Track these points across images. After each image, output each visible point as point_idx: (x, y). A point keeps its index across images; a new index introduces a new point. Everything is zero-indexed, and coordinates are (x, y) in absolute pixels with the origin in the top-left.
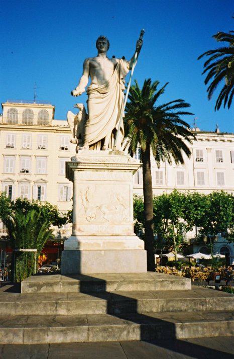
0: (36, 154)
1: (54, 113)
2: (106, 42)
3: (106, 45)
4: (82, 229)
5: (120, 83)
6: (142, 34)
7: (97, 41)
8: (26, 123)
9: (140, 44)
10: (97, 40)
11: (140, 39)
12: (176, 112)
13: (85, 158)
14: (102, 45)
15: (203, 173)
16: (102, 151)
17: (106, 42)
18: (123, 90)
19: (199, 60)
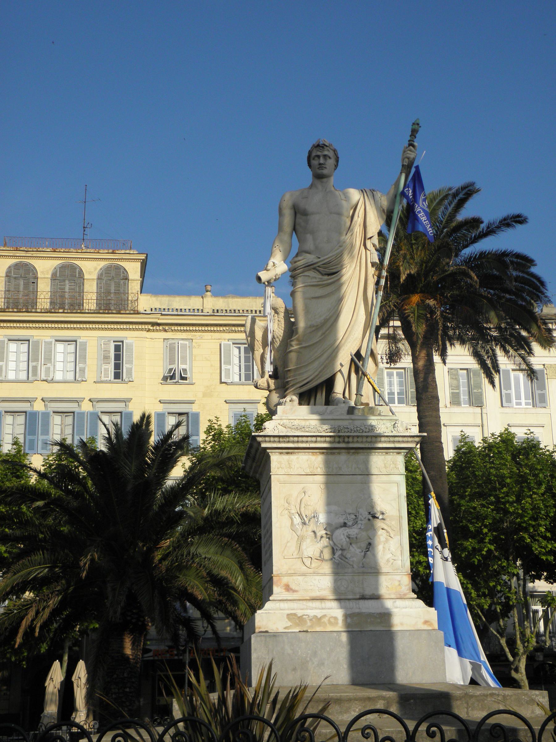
0: (45, 396)
1: (143, 275)
2: (331, 154)
3: (331, 162)
4: (293, 586)
5: (366, 248)
6: (414, 133)
7: (310, 153)
8: (62, 306)
9: (412, 155)
10: (309, 148)
11: (411, 145)
13: (296, 423)
14: (322, 161)
15: (115, 378)
16: (330, 408)
17: (331, 154)
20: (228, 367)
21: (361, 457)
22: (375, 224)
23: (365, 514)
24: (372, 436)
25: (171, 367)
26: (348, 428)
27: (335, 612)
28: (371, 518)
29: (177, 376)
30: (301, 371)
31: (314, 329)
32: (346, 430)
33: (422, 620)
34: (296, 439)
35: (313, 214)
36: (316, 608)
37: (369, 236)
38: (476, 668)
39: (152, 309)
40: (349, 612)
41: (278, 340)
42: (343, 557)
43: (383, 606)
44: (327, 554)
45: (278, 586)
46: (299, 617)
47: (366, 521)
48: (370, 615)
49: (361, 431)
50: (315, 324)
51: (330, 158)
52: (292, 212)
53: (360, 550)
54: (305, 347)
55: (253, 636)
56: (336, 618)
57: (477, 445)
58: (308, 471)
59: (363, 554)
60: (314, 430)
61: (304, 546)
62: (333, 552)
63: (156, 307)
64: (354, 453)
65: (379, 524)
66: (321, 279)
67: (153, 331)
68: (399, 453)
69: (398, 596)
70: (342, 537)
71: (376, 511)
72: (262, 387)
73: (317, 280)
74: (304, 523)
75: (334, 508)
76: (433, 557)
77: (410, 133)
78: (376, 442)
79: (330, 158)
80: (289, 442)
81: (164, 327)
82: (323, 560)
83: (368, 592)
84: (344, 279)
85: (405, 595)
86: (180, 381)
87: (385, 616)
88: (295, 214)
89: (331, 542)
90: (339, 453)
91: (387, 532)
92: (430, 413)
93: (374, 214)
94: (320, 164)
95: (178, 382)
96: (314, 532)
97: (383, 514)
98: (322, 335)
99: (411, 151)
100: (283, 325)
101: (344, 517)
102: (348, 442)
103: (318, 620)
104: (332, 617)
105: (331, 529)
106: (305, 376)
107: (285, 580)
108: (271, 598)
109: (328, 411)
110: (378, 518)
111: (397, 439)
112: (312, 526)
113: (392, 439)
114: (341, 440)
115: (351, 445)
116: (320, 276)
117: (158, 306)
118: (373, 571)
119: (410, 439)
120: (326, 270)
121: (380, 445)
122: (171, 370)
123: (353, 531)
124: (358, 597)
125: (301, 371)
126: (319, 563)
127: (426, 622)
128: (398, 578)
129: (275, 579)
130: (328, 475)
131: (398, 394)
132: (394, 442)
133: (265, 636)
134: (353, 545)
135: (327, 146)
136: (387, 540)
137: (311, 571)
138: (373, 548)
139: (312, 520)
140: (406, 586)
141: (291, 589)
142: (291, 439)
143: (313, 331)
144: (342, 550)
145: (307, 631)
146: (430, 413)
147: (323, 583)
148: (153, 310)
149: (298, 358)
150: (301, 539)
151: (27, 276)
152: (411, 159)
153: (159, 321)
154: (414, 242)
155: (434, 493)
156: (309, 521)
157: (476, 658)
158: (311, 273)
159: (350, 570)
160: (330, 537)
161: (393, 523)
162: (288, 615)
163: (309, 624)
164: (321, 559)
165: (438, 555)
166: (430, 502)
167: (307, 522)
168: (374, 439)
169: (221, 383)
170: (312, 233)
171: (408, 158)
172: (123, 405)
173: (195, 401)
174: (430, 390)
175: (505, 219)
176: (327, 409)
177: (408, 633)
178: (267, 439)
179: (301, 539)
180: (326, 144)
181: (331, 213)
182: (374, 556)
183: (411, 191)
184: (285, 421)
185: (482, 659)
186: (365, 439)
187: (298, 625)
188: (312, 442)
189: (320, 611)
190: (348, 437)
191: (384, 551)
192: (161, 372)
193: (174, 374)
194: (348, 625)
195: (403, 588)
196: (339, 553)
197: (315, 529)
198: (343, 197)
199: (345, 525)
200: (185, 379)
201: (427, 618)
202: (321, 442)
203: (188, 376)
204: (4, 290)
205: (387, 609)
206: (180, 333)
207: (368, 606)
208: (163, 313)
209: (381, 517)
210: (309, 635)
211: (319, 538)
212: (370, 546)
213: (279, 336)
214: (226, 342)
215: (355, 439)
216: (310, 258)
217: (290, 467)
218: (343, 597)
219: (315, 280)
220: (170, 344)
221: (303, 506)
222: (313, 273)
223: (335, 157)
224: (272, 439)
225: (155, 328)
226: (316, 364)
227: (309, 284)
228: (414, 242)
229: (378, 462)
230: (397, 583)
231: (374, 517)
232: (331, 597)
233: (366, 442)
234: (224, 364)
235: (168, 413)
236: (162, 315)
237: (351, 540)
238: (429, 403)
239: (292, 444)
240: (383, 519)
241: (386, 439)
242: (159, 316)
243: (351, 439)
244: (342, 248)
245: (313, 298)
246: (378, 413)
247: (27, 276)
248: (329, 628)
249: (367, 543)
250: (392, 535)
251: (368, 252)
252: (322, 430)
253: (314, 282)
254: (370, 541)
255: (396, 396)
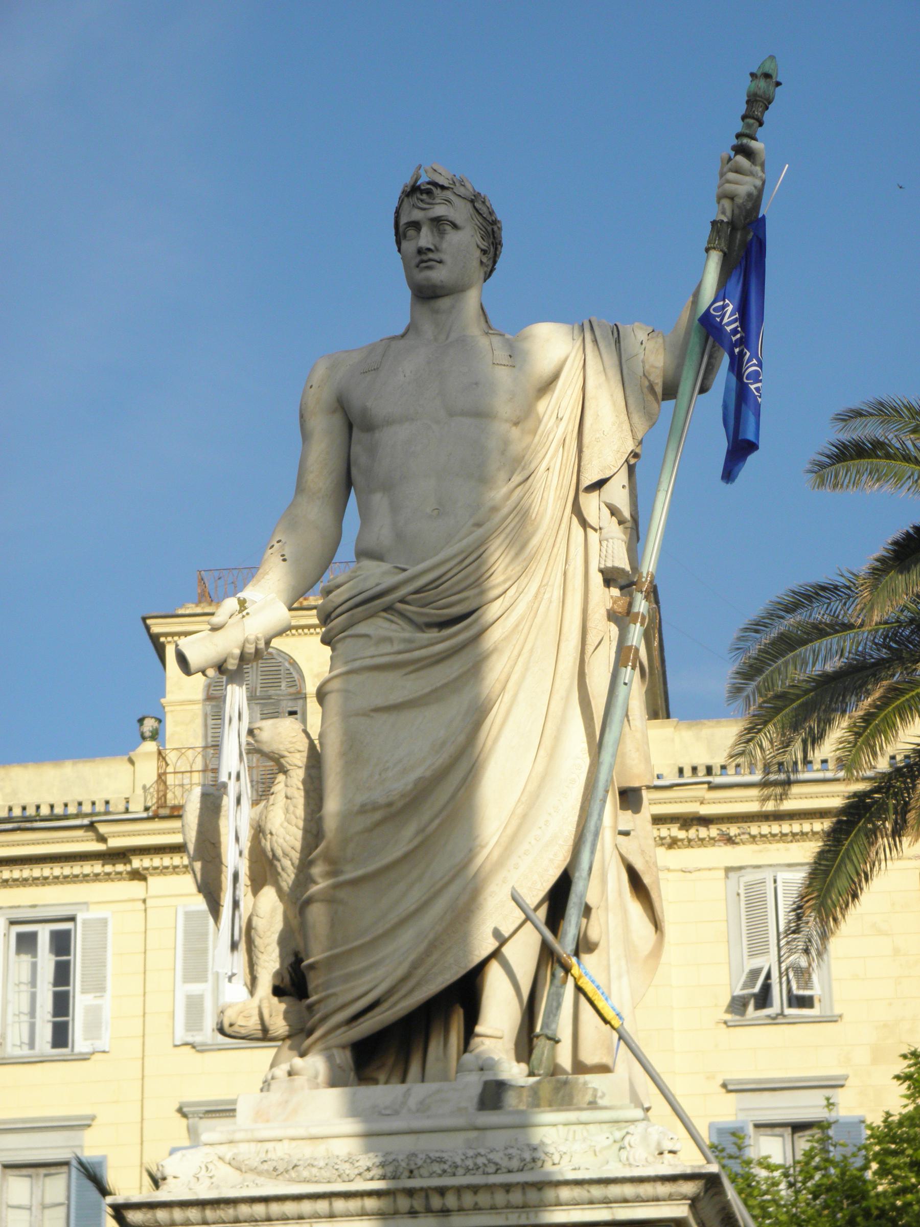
2: (459, 212)
5: (584, 523)
6: (757, 106)
17: (459, 212)
22: (612, 437)
25: (756, 963)
26: (441, 1161)
29: (777, 994)
30: (353, 967)
31: (378, 816)
32: (437, 1168)
35: (389, 422)
39: (681, 771)
41: (287, 863)
49: (491, 1169)
50: (382, 800)
51: (455, 226)
52: (337, 420)
60: (326, 1174)
63: (695, 762)
66: (409, 641)
67: (690, 843)
72: (243, 1032)
73: (396, 647)
77: (743, 108)
78: (542, 1205)
79: (455, 226)
81: (724, 827)
84: (494, 636)
86: (788, 1011)
88: (350, 426)
93: (614, 404)
95: (782, 1014)
98: (417, 834)
99: (738, 171)
106: (361, 985)
109: (412, 1102)
111: (614, 1191)
113: (597, 1192)
114: (418, 1204)
116: (408, 632)
120: (426, 610)
122: (754, 974)
125: (353, 967)
135: (443, 188)
143: (378, 824)
148: (687, 772)
149: (334, 923)
151: (272, 692)
152: (739, 201)
153: (705, 810)
158: (378, 627)
168: (532, 1195)
170: (388, 487)
171: (732, 198)
173: (846, 1078)
176: (407, 1094)
180: (442, 181)
181: (452, 414)
183: (730, 308)
184: (243, 1148)
186: (500, 1198)
190: (442, 1191)
193: (766, 988)
198: (501, 354)
204: (200, 743)
206: (781, 845)
208: (718, 780)
213: (288, 849)
216: (377, 575)
219: (387, 648)
220: (749, 886)
222: (387, 624)
223: (478, 220)
225: (692, 833)
226: (407, 936)
227: (368, 662)
235: (757, 1126)
236: (712, 787)
242: (701, 791)
243: (451, 1201)
244: (480, 531)
245: (377, 710)
246: (588, 1098)
247: (272, 692)
252: (353, 1172)
253: (384, 653)
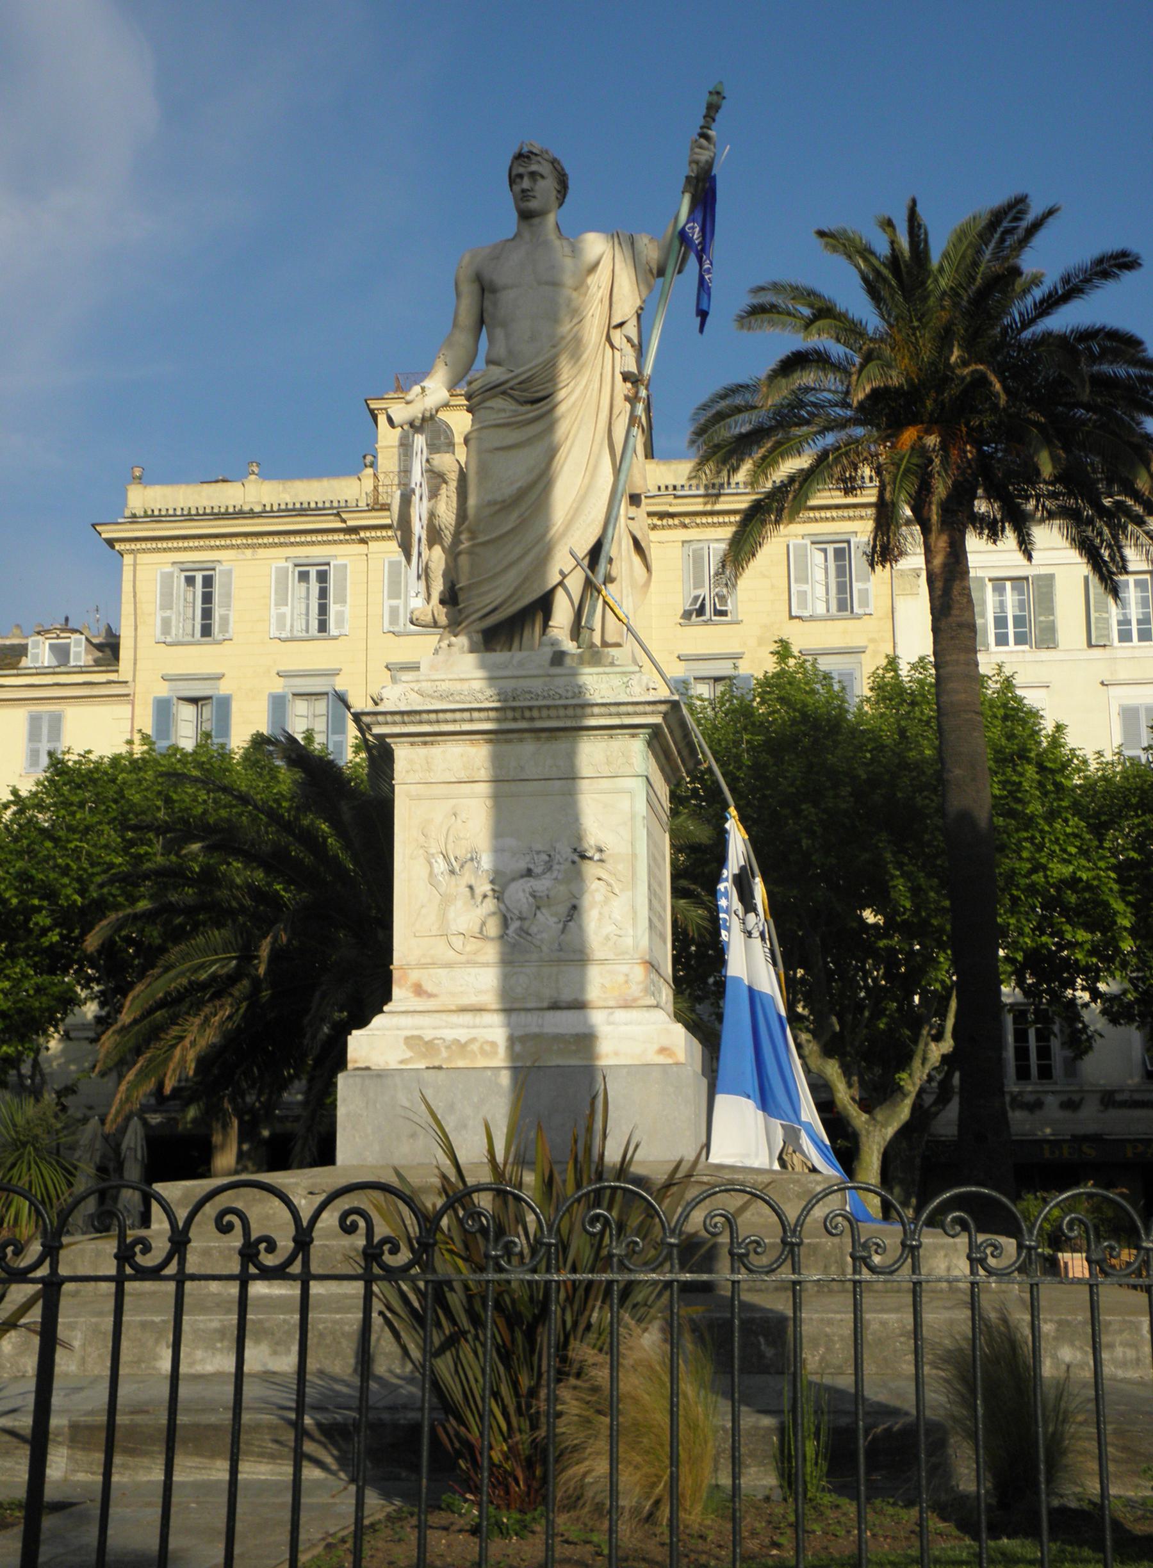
2: (544, 168)
4: (428, 987)
5: (612, 346)
6: (712, 110)
12: (610, 479)
13: (444, 686)
17: (544, 168)
18: (626, 377)
19: (907, 202)
20: (804, 587)
21: (561, 746)
23: (567, 852)
24: (575, 706)
27: (493, 1031)
28: (577, 858)
31: (497, 507)
33: (656, 1047)
34: (433, 716)
35: (505, 288)
36: (463, 1026)
37: (616, 320)
38: (791, 1136)
40: (517, 1033)
42: (524, 932)
43: (585, 1022)
44: (493, 928)
45: (400, 987)
46: (427, 1043)
47: (568, 865)
48: (557, 1038)
51: (542, 177)
52: (475, 287)
53: (555, 919)
54: (484, 544)
55: (341, 1079)
56: (493, 1044)
57: (850, 717)
58: (463, 776)
59: (561, 926)
61: (451, 914)
62: (505, 922)
64: (548, 739)
65: (591, 870)
67: (663, 527)
68: (633, 736)
69: (622, 1003)
70: (521, 894)
71: (586, 846)
74: (452, 872)
75: (510, 842)
76: (728, 929)
77: (704, 111)
78: (584, 716)
79: (542, 177)
80: (421, 722)
82: (485, 938)
83: (567, 996)
84: (562, 409)
85: (635, 1000)
87: (586, 1040)
88: (483, 290)
89: (502, 906)
90: (521, 740)
91: (609, 884)
92: (954, 657)
94: (523, 191)
96: (471, 888)
97: (601, 850)
99: (701, 147)
100: (455, 505)
101: (528, 858)
102: (532, 719)
103: (461, 1047)
104: (487, 1042)
105: (501, 883)
106: (487, 599)
107: (414, 976)
108: (385, 1008)
109: (515, 662)
110: (590, 858)
112: (468, 877)
113: (613, 709)
114: (518, 715)
115: (539, 724)
116: (514, 406)
117: (671, 482)
118: (573, 955)
119: (648, 708)
121: (593, 722)
122: (696, 598)
123: (542, 885)
124: (545, 1005)
126: (480, 944)
127: (663, 1050)
128: (624, 969)
129: (396, 975)
130: (496, 781)
131: (1139, 622)
132: (619, 715)
133: (362, 1077)
134: (544, 910)
136: (606, 900)
137: (463, 958)
138: (580, 915)
139: (468, 866)
140: (638, 983)
141: (426, 992)
142: (425, 716)
144: (521, 919)
145: (440, 1068)
146: (954, 657)
147: (482, 980)
150: (446, 900)
153: (672, 510)
154: (916, 324)
155: (736, 808)
156: (462, 867)
157: (793, 1116)
158: (498, 403)
159: (535, 956)
160: (499, 896)
161: (620, 867)
162: (407, 1038)
163: (444, 1053)
164: (482, 936)
165: (735, 924)
166: (727, 826)
167: (457, 869)
168: (579, 711)
169: (792, 617)
172: (729, 664)
174: (955, 612)
175: (1100, 261)
177: (625, 1071)
178: (380, 718)
179: (446, 900)
182: (581, 929)
184: (424, 684)
185: (804, 1118)
187: (424, 1056)
188: (464, 720)
189: (466, 1031)
190: (530, 708)
191: (600, 920)
192: (681, 602)
193: (703, 605)
194: (512, 1054)
195: (634, 987)
196: (514, 925)
197: (473, 882)
198: (567, 250)
199: (529, 873)
200: (723, 613)
201: (665, 1042)
202: (480, 720)
203: (729, 607)
205: (592, 1027)
207: (561, 1023)
209: (597, 857)
210: (441, 1074)
211: (479, 899)
212: (574, 911)
214: (800, 541)
215: (545, 713)
216: (497, 374)
217: (429, 770)
218: (516, 1006)
219: (503, 415)
220: (694, 551)
221: (451, 839)
224: (389, 718)
226: (513, 573)
228: (916, 324)
229: (592, 753)
230: (622, 979)
231: (583, 857)
232: (495, 1006)
233: (566, 717)
234: (796, 581)
236: (676, 497)
237: (539, 901)
238: (952, 638)
239: (431, 727)
240: (601, 861)
241: (603, 710)
242: (671, 499)
243: (535, 713)
244: (554, 351)
245: (498, 449)
248: (482, 1062)
249: (569, 905)
250: (617, 891)
251: (617, 354)
253: (502, 418)
254: (574, 901)
255: (1134, 627)
